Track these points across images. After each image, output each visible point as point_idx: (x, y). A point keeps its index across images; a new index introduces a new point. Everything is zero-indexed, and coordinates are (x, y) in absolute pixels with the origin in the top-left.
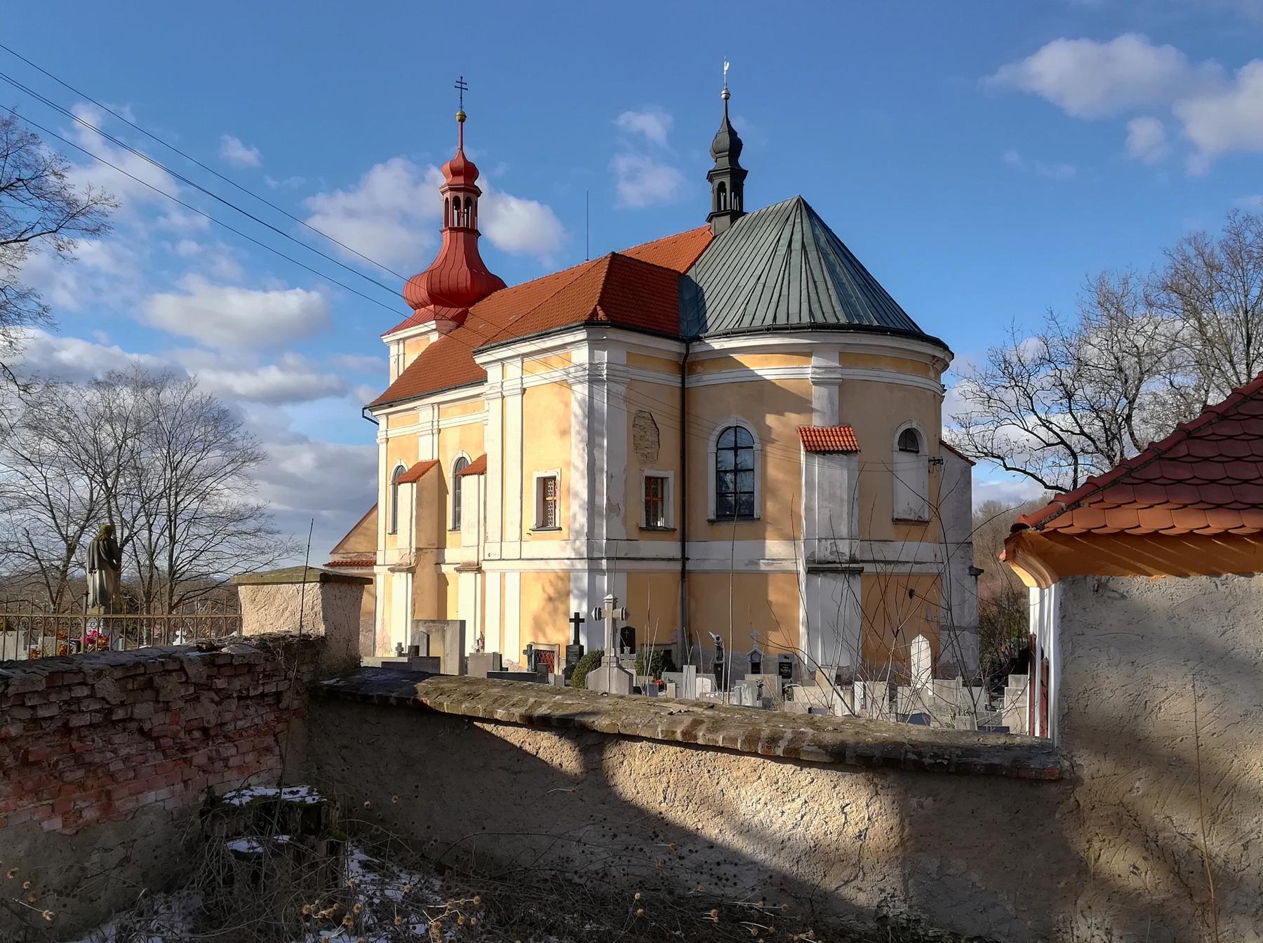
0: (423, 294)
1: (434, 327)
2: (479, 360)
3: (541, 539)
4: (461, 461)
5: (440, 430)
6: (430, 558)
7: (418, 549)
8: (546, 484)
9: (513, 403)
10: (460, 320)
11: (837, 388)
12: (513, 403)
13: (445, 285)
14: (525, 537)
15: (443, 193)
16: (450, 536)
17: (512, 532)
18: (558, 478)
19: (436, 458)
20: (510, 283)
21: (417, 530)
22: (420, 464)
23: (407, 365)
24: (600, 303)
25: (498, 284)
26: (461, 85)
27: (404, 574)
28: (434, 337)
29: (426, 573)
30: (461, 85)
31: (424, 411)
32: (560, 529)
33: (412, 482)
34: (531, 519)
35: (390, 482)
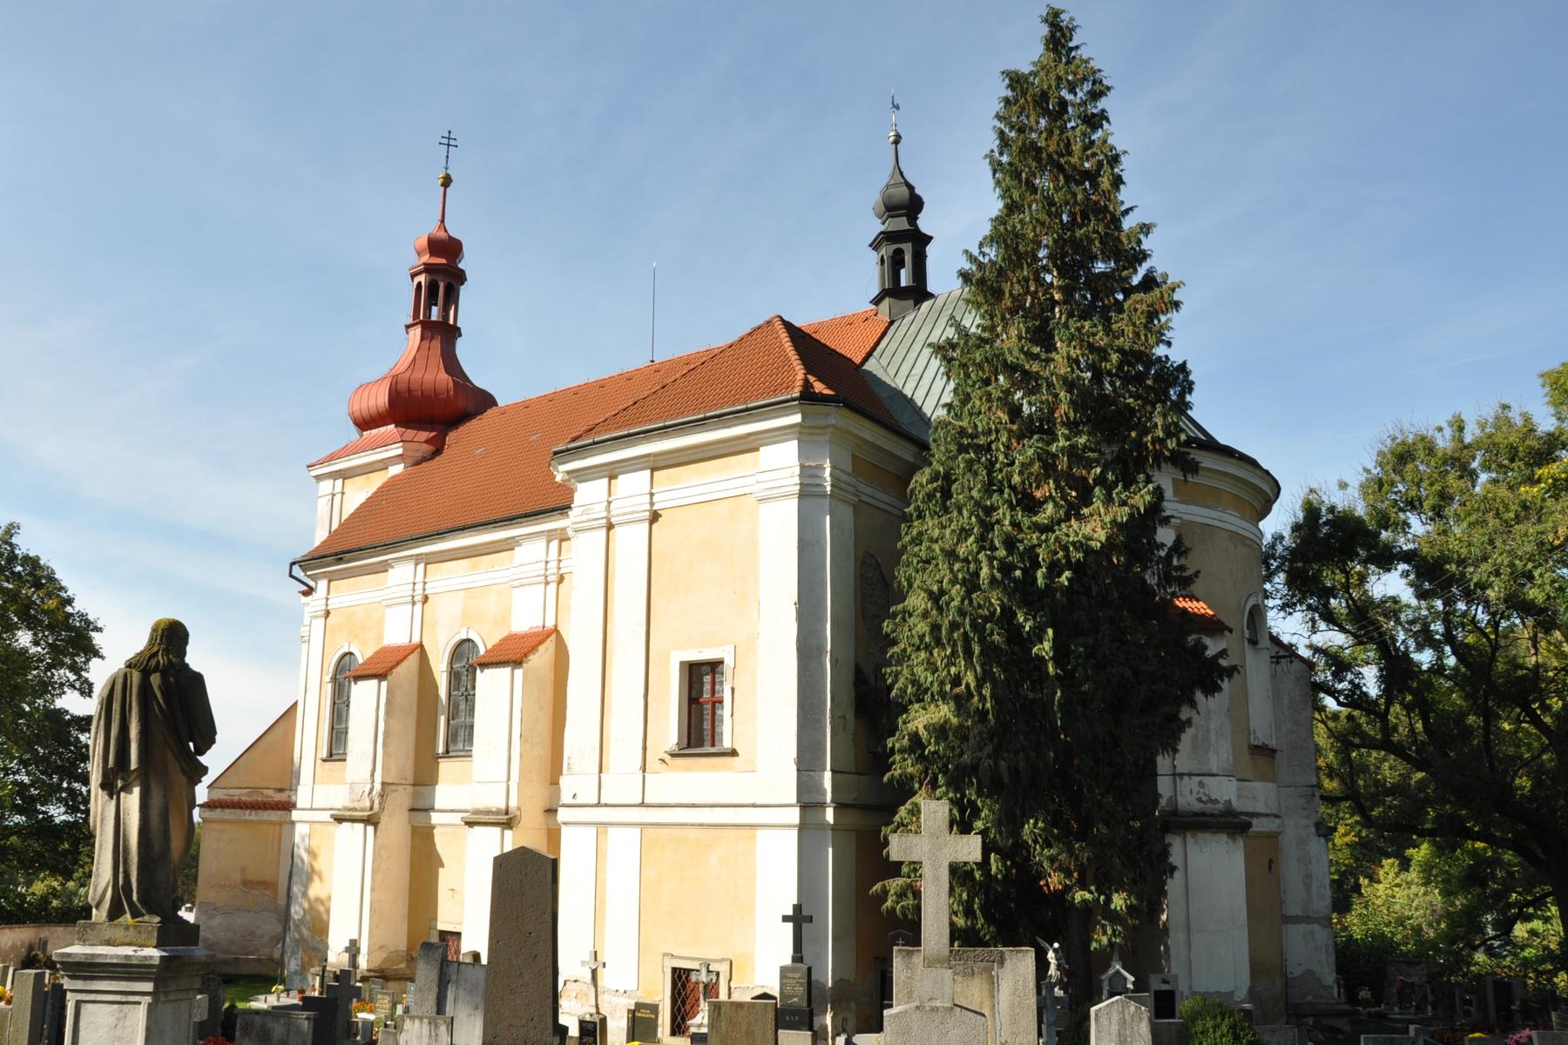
0: (381, 399)
1: (400, 451)
2: (561, 472)
3: (688, 769)
4: (462, 649)
5: (426, 599)
6: (401, 799)
7: (383, 784)
8: (700, 679)
9: (631, 539)
10: (438, 448)
11: (437, 806)
12: (631, 539)
13: (365, 414)
14: (652, 762)
15: (413, 276)
16: (445, 767)
17: (625, 751)
18: (729, 662)
19: (416, 640)
20: (501, 403)
21: (385, 753)
22: (384, 652)
23: (345, 517)
24: (809, 369)
25: (485, 401)
26: (449, 142)
27: (360, 826)
28: (397, 469)
29: (396, 824)
30: (449, 142)
31: (402, 574)
32: (734, 753)
33: (381, 677)
34: (669, 729)
35: (327, 678)
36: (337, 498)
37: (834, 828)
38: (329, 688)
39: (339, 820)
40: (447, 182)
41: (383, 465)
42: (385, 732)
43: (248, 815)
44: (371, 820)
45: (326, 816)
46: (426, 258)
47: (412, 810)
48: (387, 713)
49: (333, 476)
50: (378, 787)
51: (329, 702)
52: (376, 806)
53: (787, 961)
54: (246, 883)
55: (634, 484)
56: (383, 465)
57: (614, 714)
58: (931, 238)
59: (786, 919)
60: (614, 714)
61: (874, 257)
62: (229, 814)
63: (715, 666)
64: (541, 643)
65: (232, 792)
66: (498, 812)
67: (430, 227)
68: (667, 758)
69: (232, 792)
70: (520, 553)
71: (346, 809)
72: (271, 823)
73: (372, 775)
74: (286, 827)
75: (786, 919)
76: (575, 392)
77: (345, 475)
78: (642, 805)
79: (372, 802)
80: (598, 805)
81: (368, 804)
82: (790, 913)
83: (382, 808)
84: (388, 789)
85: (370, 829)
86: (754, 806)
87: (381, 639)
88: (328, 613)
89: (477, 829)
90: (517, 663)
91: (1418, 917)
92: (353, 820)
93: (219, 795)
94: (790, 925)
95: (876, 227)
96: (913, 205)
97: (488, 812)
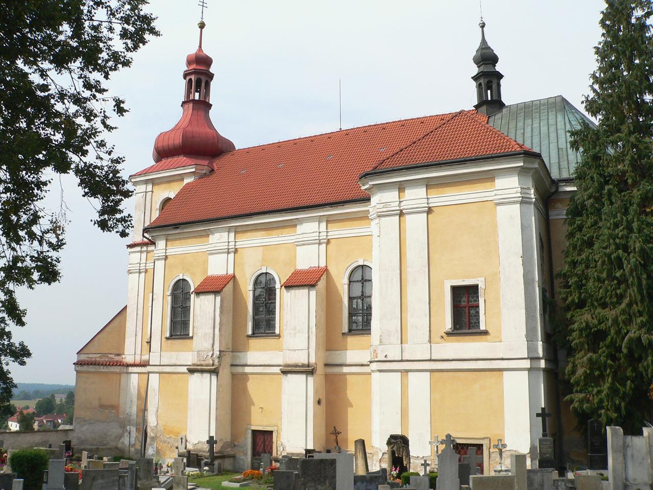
1: (193, 170)
3: (458, 341)
5: (236, 251)
7: (220, 351)
9: (416, 224)
19: (231, 272)
21: (220, 335)
23: (153, 219)
26: (202, 26)
27: (207, 376)
28: (187, 180)
29: (225, 372)
31: (220, 238)
32: (486, 333)
33: (216, 292)
35: (169, 293)
36: (149, 195)
37: (544, 370)
38: (169, 298)
39: (191, 371)
40: (202, 26)
41: (181, 178)
42: (221, 324)
43: (102, 369)
44: (214, 372)
45: (184, 369)
46: (194, 66)
47: (232, 365)
48: (221, 312)
49: (146, 182)
50: (217, 353)
51: (169, 307)
52: (216, 362)
53: (541, 436)
54: (102, 406)
55: (416, 196)
56: (181, 178)
57: (407, 313)
58: (503, 76)
59: (538, 415)
60: (407, 313)
61: (474, 84)
62: (91, 368)
63: (473, 290)
64: (321, 276)
65: (91, 356)
66: (303, 365)
67: (193, 50)
68: (445, 335)
69: (91, 356)
70: (301, 229)
71: (194, 365)
72: (116, 373)
73: (213, 346)
74: (124, 377)
75: (538, 415)
76: (295, 142)
77: (153, 182)
78: (430, 360)
79: (213, 361)
80: (402, 361)
81: (211, 362)
82: (540, 412)
83: (220, 365)
84: (222, 354)
85: (214, 378)
86: (502, 359)
87: (206, 270)
88: (166, 258)
89: (290, 376)
90: (312, 286)
91: (149, 452)
92: (202, 371)
93: (83, 357)
94: (540, 418)
95: (475, 70)
96: (494, 59)
97: (296, 366)
